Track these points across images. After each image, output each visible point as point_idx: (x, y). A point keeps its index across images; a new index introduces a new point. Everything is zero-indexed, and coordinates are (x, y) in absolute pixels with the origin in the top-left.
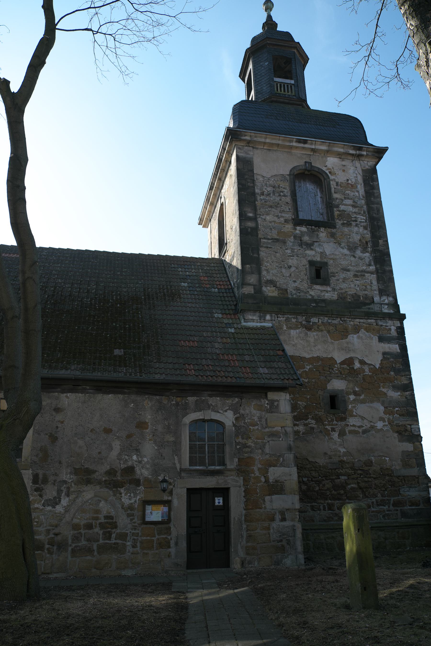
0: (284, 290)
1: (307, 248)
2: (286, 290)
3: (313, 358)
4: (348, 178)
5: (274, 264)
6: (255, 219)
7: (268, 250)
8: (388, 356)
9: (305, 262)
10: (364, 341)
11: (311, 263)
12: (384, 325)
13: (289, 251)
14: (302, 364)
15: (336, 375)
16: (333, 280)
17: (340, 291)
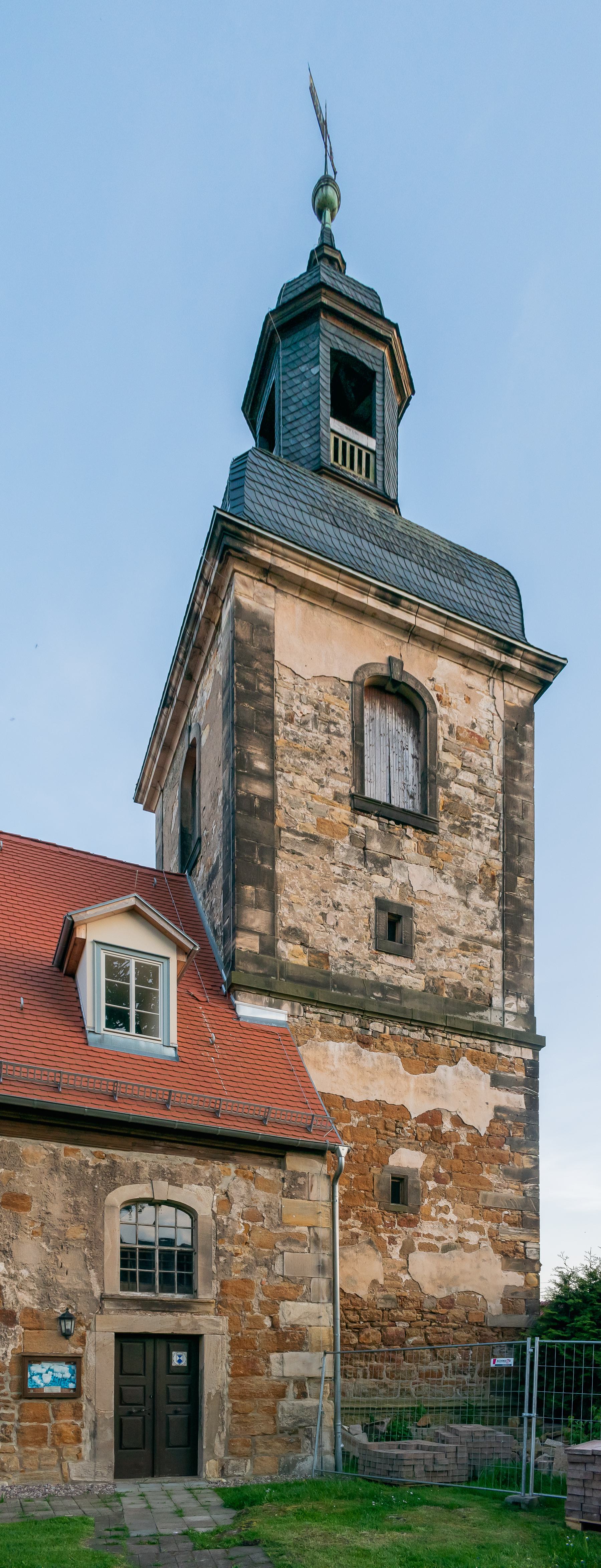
0: (321, 954)
2: (326, 955)
3: (368, 1103)
7: (294, 860)
8: (504, 1115)
10: (464, 1081)
11: (381, 904)
12: (503, 1053)
13: (337, 870)
15: (407, 1141)
16: (419, 950)
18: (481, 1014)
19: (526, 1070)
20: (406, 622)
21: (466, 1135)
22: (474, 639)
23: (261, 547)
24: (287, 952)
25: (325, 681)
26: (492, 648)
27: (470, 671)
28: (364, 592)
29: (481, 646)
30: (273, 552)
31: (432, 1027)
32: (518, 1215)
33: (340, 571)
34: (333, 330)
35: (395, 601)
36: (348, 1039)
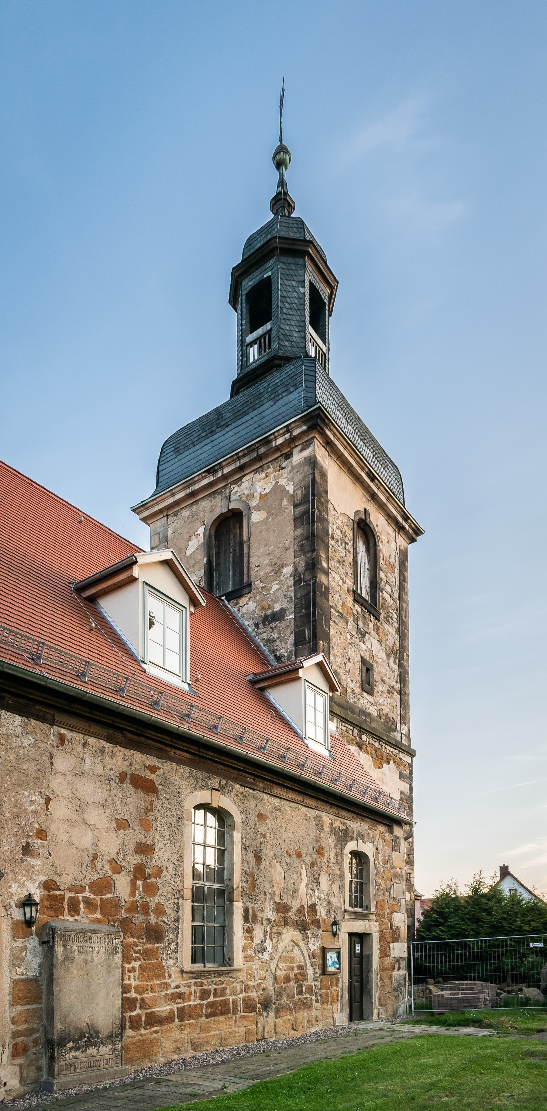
20: (374, 491)
22: (396, 508)
23: (330, 430)
28: (363, 469)
30: (334, 435)
34: (311, 269)
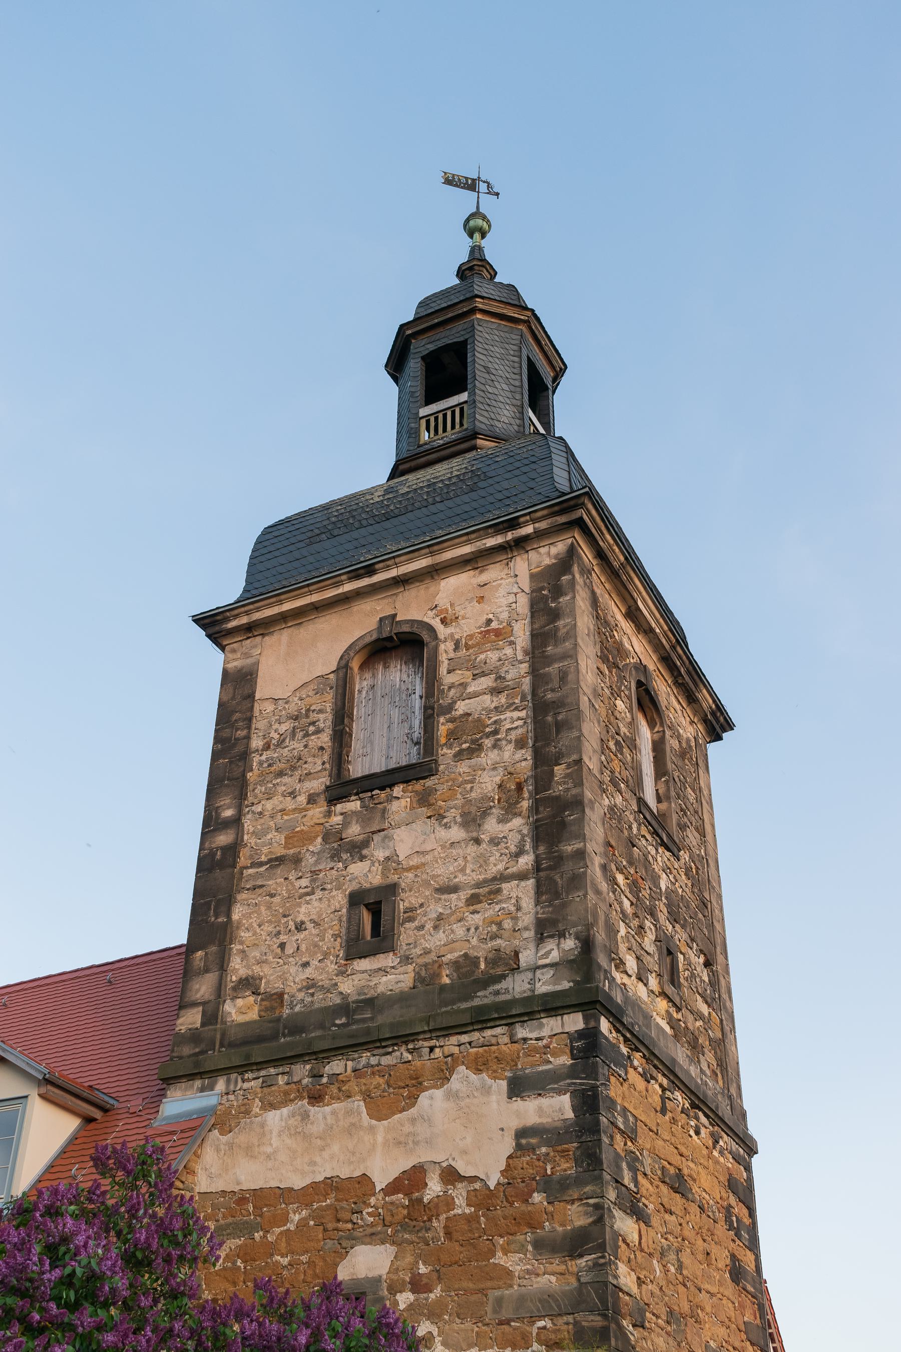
0: (275, 997)
1: (350, 859)
2: (281, 995)
3: (314, 1185)
4: (491, 616)
5: (262, 930)
6: (236, 822)
7: (253, 896)
8: (533, 1141)
9: (340, 899)
10: (463, 1104)
12: (530, 1036)
13: (304, 882)
14: (282, 1209)
15: (370, 1230)
16: (406, 935)
17: (421, 961)
18: (497, 987)
19: (572, 1049)
21: (465, 1194)
22: (468, 542)
23: (236, 616)
24: (233, 1011)
25: (307, 686)
26: (492, 537)
27: (482, 569)
29: (478, 544)
30: (247, 613)
31: (412, 1038)
32: (567, 1324)
33: (308, 585)
35: (370, 570)
36: (295, 1099)
